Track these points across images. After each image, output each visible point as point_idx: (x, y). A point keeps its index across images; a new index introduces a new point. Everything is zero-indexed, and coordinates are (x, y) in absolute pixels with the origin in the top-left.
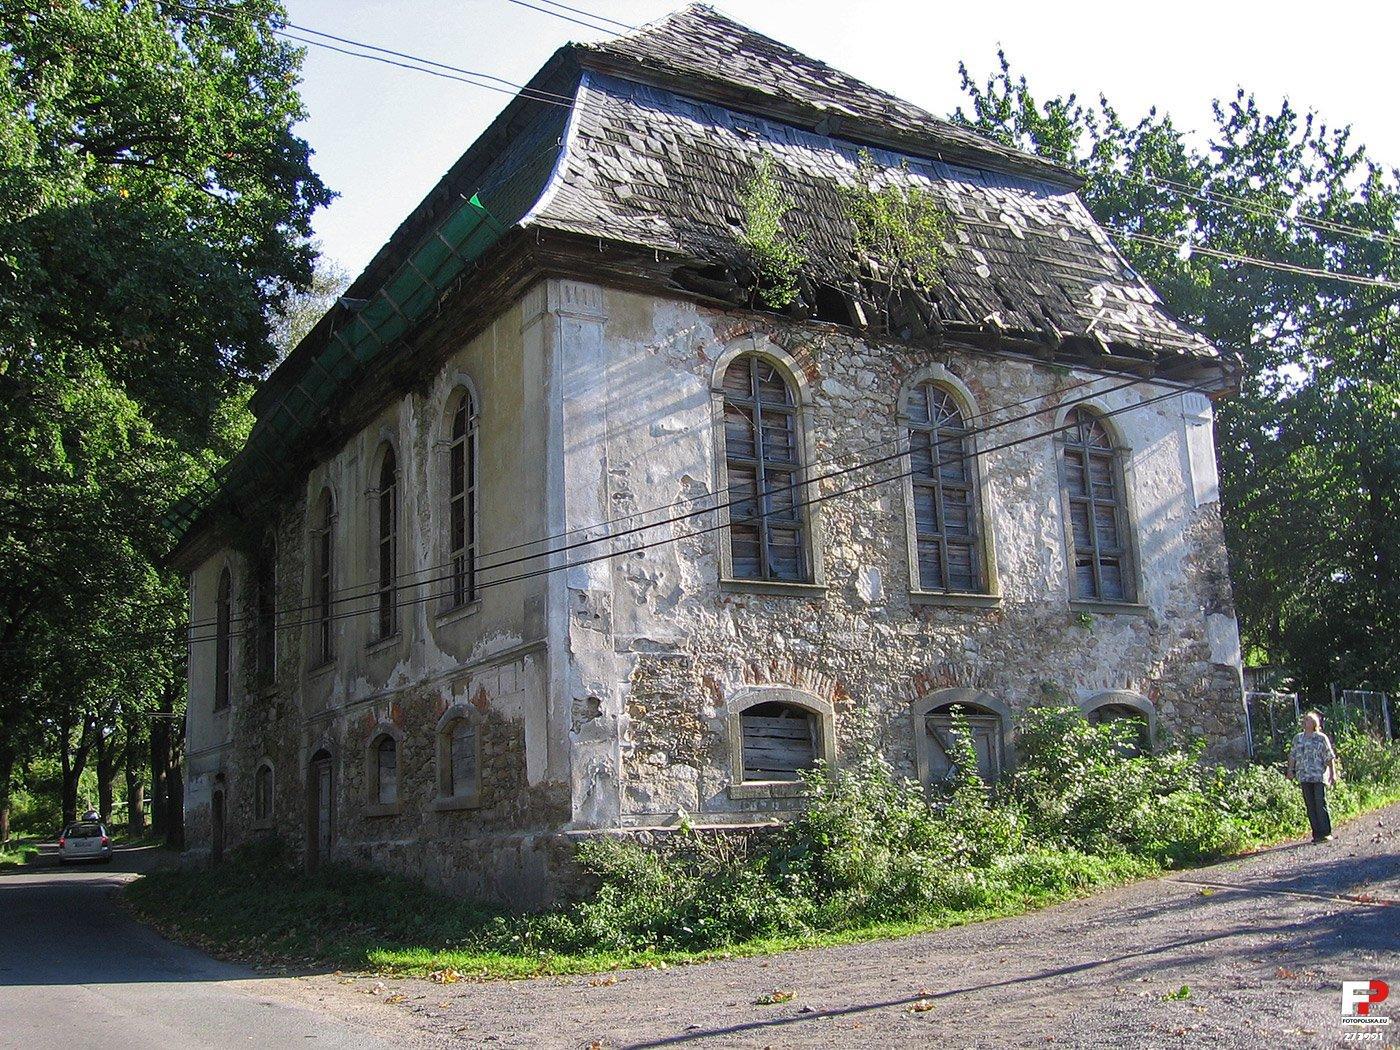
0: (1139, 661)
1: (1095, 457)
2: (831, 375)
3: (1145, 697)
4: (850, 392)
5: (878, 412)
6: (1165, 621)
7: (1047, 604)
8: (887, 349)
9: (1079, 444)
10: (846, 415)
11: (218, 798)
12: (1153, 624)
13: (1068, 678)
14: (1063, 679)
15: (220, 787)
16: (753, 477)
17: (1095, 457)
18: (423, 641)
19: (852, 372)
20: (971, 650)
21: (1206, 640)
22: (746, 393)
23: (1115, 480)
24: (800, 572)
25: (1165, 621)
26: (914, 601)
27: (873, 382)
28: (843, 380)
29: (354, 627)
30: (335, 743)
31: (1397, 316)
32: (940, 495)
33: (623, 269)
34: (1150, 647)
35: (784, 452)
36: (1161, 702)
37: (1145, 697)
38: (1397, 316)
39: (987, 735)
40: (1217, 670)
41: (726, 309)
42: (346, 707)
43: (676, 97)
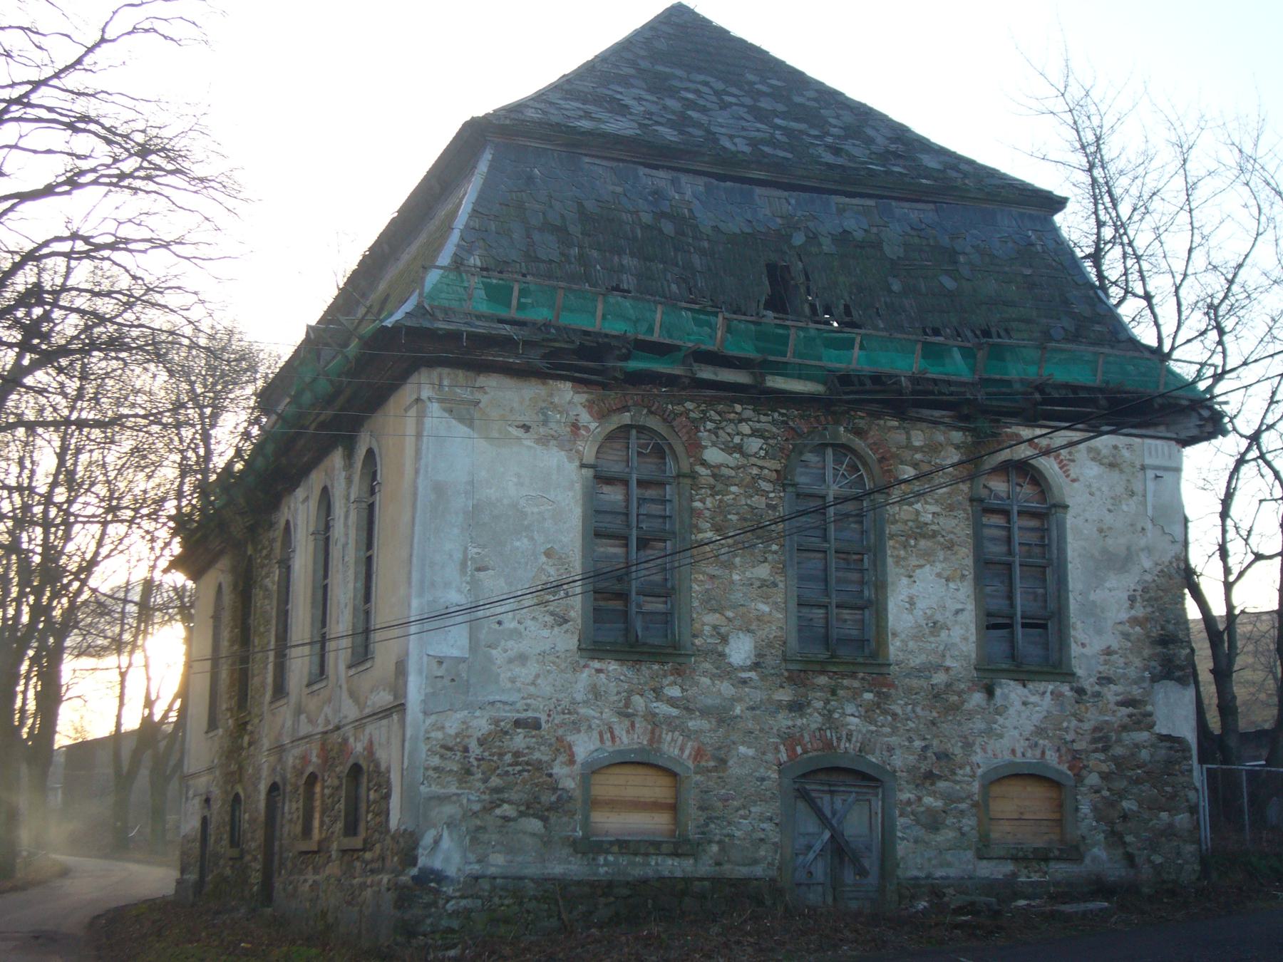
0: (1060, 730)
1: (1024, 513)
2: (714, 445)
3: (1064, 768)
4: (734, 459)
5: (765, 479)
6: (1097, 688)
7: (947, 669)
8: (780, 414)
9: (1008, 502)
10: (727, 481)
11: (205, 822)
12: (1080, 691)
13: (968, 746)
14: (962, 747)
15: (206, 813)
16: (626, 546)
17: (1024, 513)
18: (340, 687)
19: (737, 440)
20: (853, 715)
21: (1149, 708)
22: (625, 464)
23: (1049, 539)
24: (669, 636)
25: (1097, 688)
26: (791, 667)
27: (761, 448)
28: (730, 449)
29: (300, 664)
30: (284, 778)
31: (63, 738)
32: (832, 558)
33: (493, 355)
34: (1074, 715)
35: (661, 520)
36: (1084, 772)
37: (1064, 768)
38: (63, 738)
39: (869, 801)
40: (1162, 741)
41: (604, 386)
42: (293, 742)
43: (587, 160)
